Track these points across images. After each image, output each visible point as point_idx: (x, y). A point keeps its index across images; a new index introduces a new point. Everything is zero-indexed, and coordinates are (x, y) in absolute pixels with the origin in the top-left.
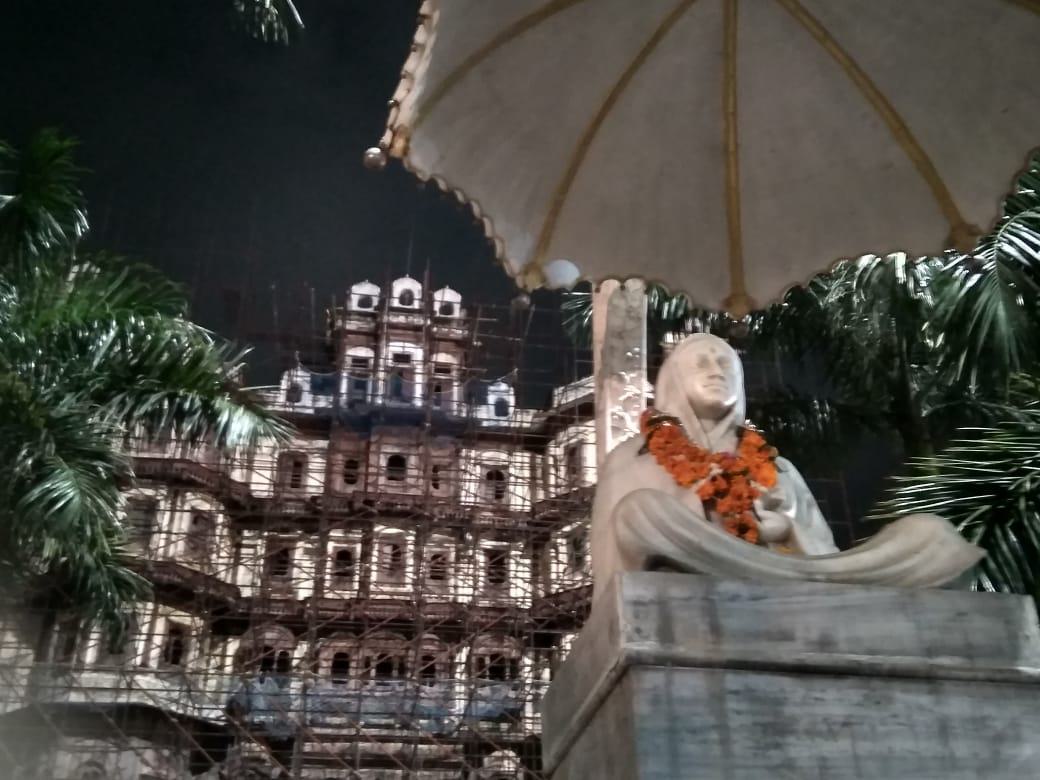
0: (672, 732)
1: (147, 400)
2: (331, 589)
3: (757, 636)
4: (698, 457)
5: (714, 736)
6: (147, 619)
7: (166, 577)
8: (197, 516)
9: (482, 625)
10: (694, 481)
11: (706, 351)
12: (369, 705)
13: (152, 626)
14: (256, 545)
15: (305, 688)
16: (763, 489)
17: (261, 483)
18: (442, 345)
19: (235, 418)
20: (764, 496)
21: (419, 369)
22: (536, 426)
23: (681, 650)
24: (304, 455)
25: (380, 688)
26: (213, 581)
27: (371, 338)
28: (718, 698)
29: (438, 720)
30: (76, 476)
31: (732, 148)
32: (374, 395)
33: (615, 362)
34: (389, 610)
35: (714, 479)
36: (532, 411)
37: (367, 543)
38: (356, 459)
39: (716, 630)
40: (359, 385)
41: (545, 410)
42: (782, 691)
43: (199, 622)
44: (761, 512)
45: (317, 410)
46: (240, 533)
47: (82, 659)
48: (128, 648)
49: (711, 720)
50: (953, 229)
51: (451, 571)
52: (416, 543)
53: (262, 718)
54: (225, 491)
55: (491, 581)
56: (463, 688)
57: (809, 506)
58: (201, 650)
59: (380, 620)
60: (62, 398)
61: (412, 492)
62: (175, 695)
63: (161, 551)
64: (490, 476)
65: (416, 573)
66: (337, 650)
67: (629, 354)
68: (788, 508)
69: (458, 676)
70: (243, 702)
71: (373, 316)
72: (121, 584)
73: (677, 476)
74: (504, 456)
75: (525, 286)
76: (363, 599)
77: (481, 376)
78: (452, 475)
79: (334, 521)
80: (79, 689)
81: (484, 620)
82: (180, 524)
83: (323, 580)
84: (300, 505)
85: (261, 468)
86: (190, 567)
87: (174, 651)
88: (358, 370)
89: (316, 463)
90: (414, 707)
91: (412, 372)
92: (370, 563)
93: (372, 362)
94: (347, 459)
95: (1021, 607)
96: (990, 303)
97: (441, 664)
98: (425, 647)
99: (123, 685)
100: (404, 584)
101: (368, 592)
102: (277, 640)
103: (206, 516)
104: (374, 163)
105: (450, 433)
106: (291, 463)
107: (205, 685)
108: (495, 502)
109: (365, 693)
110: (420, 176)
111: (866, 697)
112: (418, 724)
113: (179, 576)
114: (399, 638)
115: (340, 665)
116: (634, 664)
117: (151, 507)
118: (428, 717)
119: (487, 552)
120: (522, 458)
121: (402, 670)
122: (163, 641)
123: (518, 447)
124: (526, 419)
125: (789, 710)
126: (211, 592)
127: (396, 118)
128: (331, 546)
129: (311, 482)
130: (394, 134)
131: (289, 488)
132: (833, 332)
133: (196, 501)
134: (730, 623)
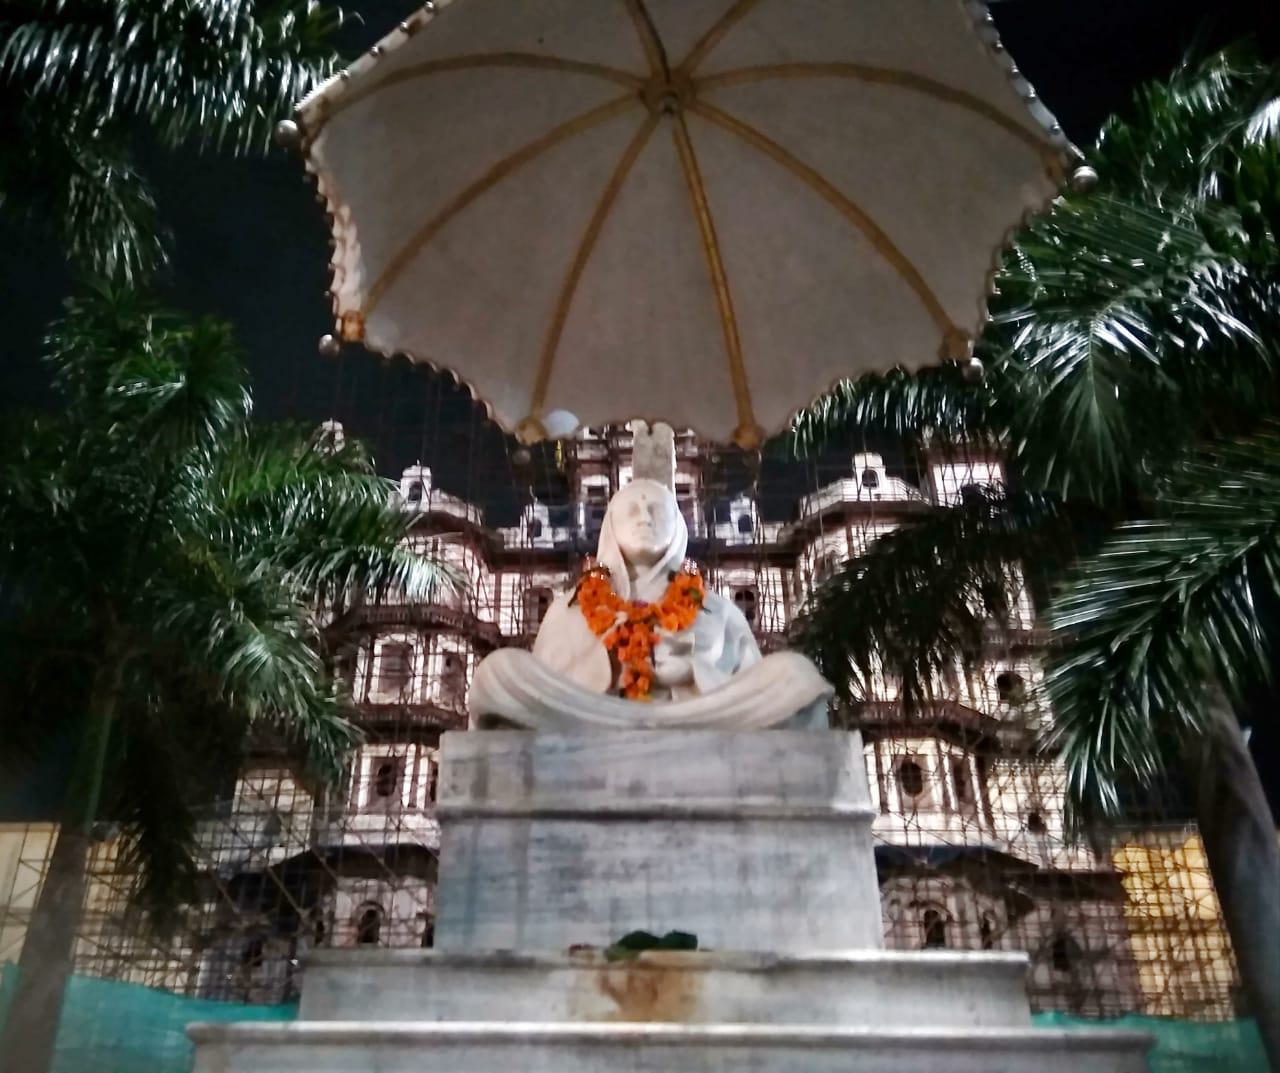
0: (472, 880)
5: (512, 882)
8: (451, 658)
24: (549, 590)
28: (521, 846)
31: (719, 278)
36: (779, 525)
39: (529, 782)
41: (792, 522)
49: (511, 868)
74: (751, 575)
75: (524, 441)
77: (722, 493)
80: (353, 832)
88: (596, 499)
93: (608, 490)
96: (1082, 400)
99: (393, 827)
106: (536, 599)
110: (386, 355)
111: (668, 840)
117: (405, 651)
120: (773, 574)
124: (771, 534)
125: (588, 855)
133: (446, 643)
134: (543, 775)
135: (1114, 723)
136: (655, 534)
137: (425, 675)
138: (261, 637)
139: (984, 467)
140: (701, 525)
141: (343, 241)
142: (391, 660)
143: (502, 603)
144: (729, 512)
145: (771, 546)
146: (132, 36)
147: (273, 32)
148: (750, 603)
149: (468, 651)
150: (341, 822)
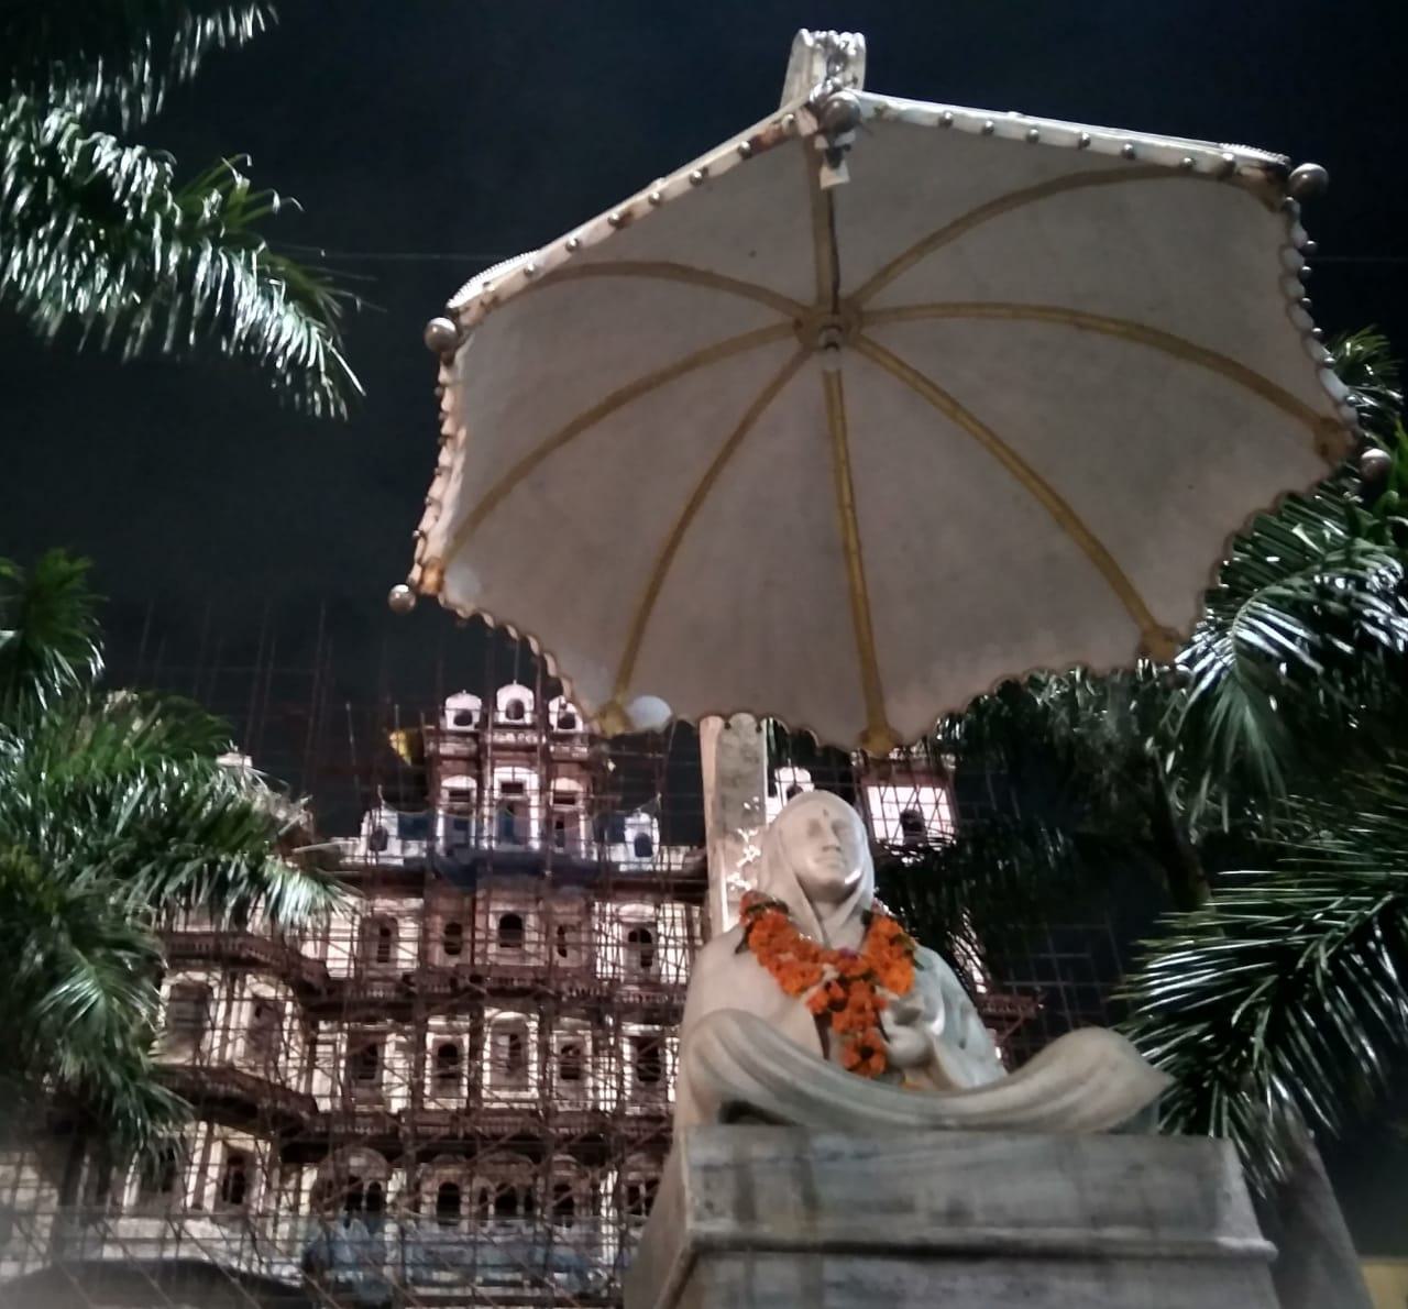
1: (181, 870)
2: (432, 1098)
3: (865, 1207)
4: (811, 955)
6: (199, 1144)
7: (222, 1088)
8: (260, 1005)
9: (631, 1142)
10: (803, 989)
11: (817, 814)
12: (490, 1255)
13: (207, 1153)
14: (334, 1041)
15: (402, 1232)
16: (893, 996)
17: (339, 961)
18: (562, 768)
19: (289, 888)
20: (894, 1006)
21: (535, 800)
22: (691, 868)
23: (767, 1230)
24: (394, 920)
25: (502, 1231)
26: (284, 1091)
27: (473, 764)
29: (581, 1274)
30: (97, 972)
31: (853, 545)
32: (479, 838)
33: (731, 818)
34: (509, 1124)
35: (828, 986)
36: (684, 849)
37: (476, 1033)
38: (458, 922)
39: (811, 1202)
40: (459, 824)
42: (899, 1280)
43: (265, 1147)
44: (890, 1027)
45: (406, 860)
46: (315, 1026)
47: (118, 1200)
48: (177, 1183)
50: (1145, 634)
51: (589, 1068)
52: (541, 1032)
53: (350, 1274)
54: (294, 971)
55: (641, 1079)
56: (611, 1229)
57: (964, 1013)
58: (269, 1185)
59: (496, 1137)
60: (78, 873)
61: (533, 962)
62: (236, 1246)
63: (215, 1053)
64: (632, 937)
65: (542, 1071)
66: (444, 1180)
67: (747, 806)
68: (932, 1018)
69: (604, 1212)
70: (323, 1253)
71: (475, 736)
72: (154, 1108)
73: (783, 982)
74: (649, 910)
76: (474, 1109)
77: (614, 805)
78: (584, 938)
79: (433, 1005)
80: (116, 1241)
81: (635, 1134)
82: (239, 1017)
83: (422, 1085)
84: (390, 985)
85: (337, 939)
86: (252, 1073)
87: (235, 1188)
88: (459, 805)
89: (408, 929)
90: (547, 1256)
91: (526, 805)
92: (482, 1061)
93: (474, 794)
94: (448, 921)
95: (1220, 1157)
96: (1232, 712)
97: (580, 1195)
98: (558, 1173)
99: (170, 1235)
100: (527, 1088)
101: (480, 1100)
102: (366, 1169)
103: (271, 1004)
104: (403, 603)
105: (579, 882)
106: (377, 932)
107: (275, 1231)
108: (642, 971)
109: (481, 1238)
110: (460, 612)
112: (552, 1279)
113: (239, 1086)
114: (523, 1162)
115: (449, 1201)
116: (704, 1251)
117: (202, 995)
118: (567, 1270)
119: (634, 1040)
120: (674, 911)
121: (530, 1205)
122: (220, 1174)
123: (668, 897)
126: (280, 1105)
127: (423, 552)
128: (430, 1038)
129: (402, 954)
130: (424, 568)
131: (374, 964)
132: (1056, 740)
133: (260, 986)
134: (829, 1192)
135: (1225, 1119)
136: (845, 862)
137: (226, 1029)
138: (89, 968)
139: (930, 790)
140: (589, 844)
141: (450, 469)
142: (183, 1005)
143: (332, 935)
144: (623, 829)
145: (678, 875)
146: (21, 201)
147: (192, 215)
148: (646, 947)
149: (287, 998)
150: (101, 1227)
